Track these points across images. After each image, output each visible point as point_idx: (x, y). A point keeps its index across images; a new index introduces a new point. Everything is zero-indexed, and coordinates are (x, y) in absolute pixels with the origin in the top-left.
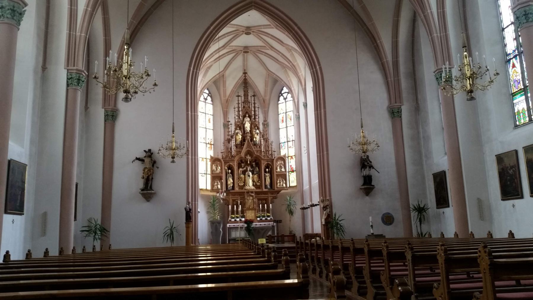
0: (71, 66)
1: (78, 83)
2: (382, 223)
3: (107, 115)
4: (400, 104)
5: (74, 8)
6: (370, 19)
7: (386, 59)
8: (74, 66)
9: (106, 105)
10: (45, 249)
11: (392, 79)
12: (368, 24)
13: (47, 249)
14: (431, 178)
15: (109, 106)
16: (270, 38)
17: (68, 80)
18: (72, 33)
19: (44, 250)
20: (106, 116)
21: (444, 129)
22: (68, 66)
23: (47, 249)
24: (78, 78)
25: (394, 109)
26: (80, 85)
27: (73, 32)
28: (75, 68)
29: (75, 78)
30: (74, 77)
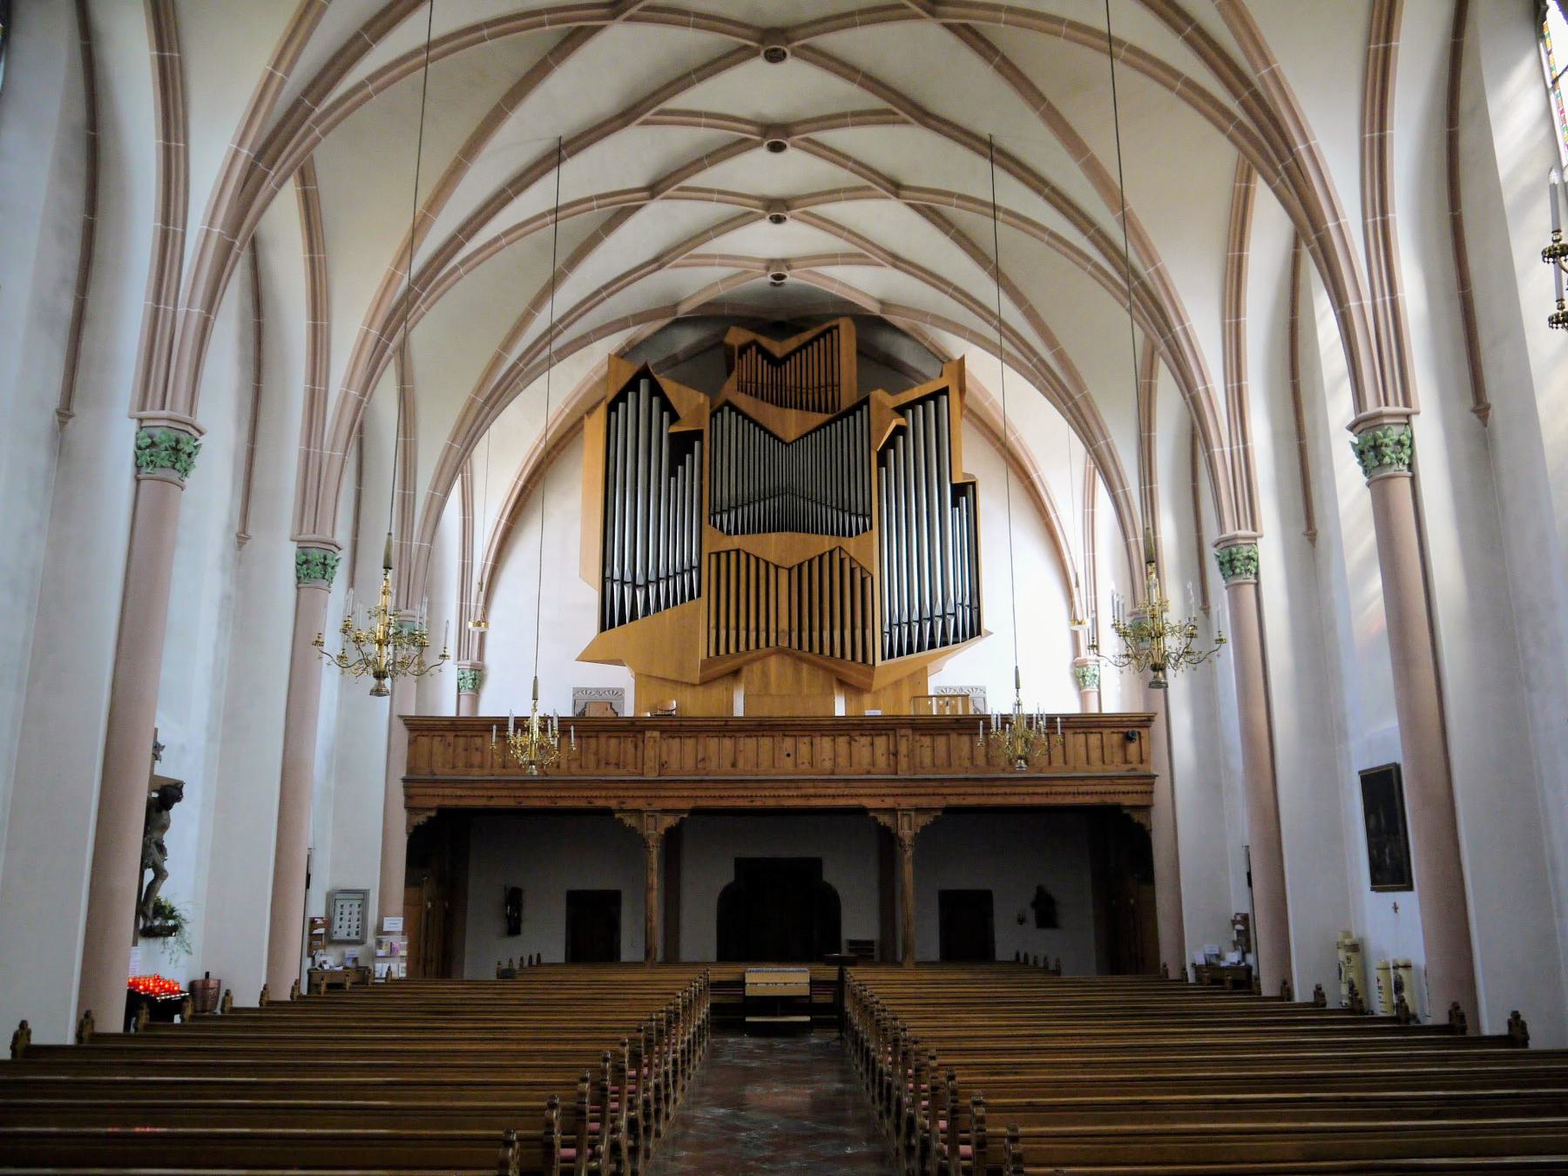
0: (152, 408)
1: (173, 459)
2: (840, 892)
3: (306, 562)
4: (1253, 533)
5: (1372, 132)
6: (1150, 257)
7: (346, 392)
8: (163, 408)
9: (304, 531)
10: (19, 1022)
11: (1227, 449)
12: (1146, 273)
13: (23, 1025)
14: (1357, 780)
15: (314, 532)
16: (565, 328)
17: (139, 452)
18: (162, 306)
19: (16, 1027)
20: (303, 563)
21: (381, 563)
22: (143, 408)
23: (23, 1025)
24: (1372, 443)
25: (1234, 550)
26: (178, 466)
27: (166, 304)
28: (164, 413)
29: (163, 446)
30: (161, 443)
